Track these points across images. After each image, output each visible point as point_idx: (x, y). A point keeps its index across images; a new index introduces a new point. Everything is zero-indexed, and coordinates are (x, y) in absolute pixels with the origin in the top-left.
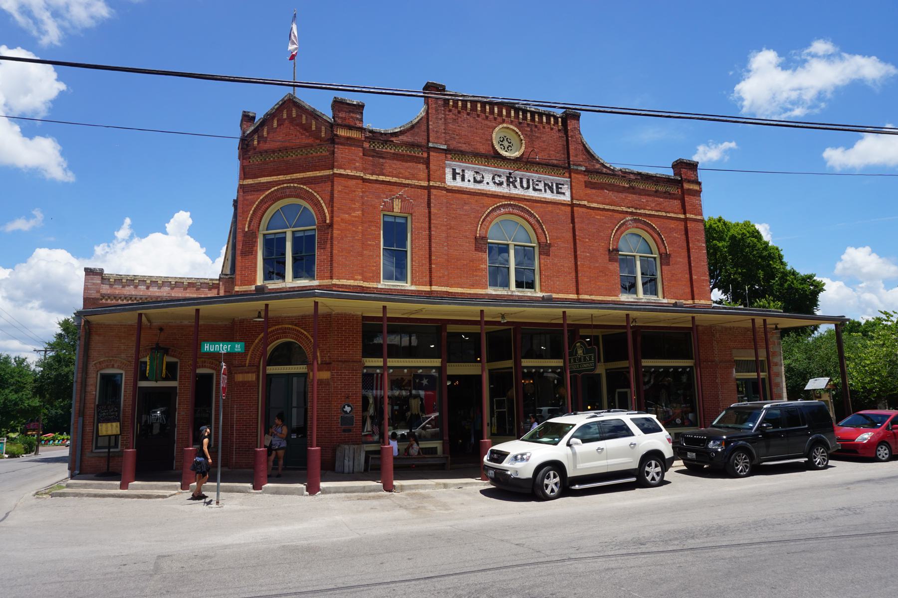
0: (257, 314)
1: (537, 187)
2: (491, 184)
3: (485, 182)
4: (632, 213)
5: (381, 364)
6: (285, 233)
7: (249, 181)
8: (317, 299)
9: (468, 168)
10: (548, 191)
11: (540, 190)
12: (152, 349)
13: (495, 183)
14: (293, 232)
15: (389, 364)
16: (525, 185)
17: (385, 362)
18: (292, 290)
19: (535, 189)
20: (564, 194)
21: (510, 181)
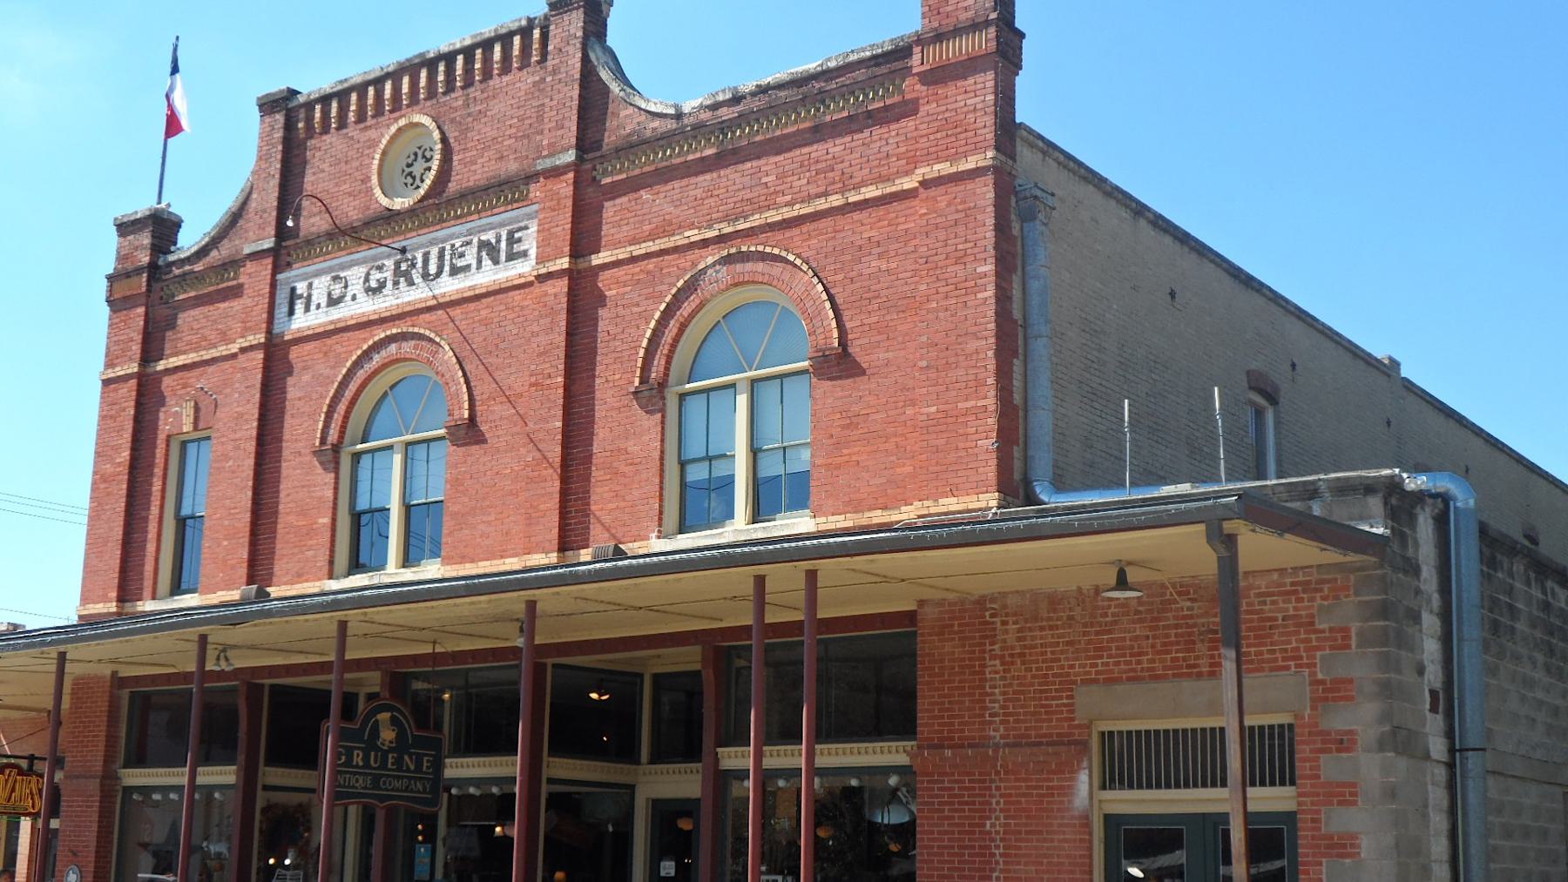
1: (460, 263)
2: (361, 297)
3: (348, 298)
10: (487, 262)
11: (468, 267)
16: (433, 269)
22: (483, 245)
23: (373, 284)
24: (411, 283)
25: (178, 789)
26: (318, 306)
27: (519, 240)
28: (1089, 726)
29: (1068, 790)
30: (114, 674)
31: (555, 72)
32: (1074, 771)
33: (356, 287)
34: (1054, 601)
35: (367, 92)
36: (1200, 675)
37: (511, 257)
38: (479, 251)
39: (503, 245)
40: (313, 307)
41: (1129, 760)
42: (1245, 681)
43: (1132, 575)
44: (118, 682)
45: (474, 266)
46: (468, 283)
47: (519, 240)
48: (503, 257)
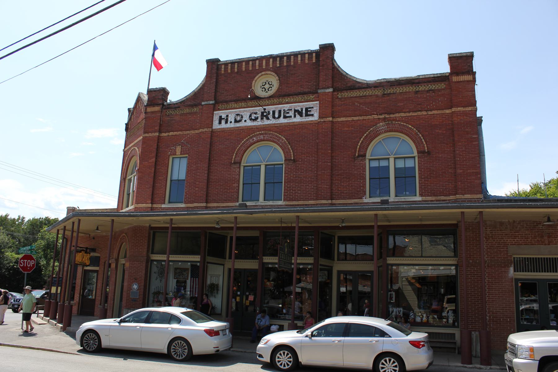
0: (546, 219)
1: (287, 115)
2: (248, 121)
3: (243, 121)
4: (384, 119)
5: (165, 259)
6: (260, 166)
7: (470, 109)
8: (80, 218)
9: (230, 113)
10: (298, 116)
11: (291, 117)
12: (406, 247)
13: (251, 119)
14: (266, 165)
15: (170, 259)
16: (277, 115)
17: (168, 257)
18: (263, 207)
19: (285, 117)
20: (312, 115)
21: (265, 115)
22: (295, 111)
23: (253, 118)
24: (268, 119)
25: (164, 261)
26: (231, 122)
27: (310, 111)
28: (511, 256)
29: (507, 272)
30: (150, 225)
31: (323, 66)
32: (509, 267)
33: (246, 117)
34: (501, 224)
35: (249, 64)
36: (545, 244)
37: (307, 115)
38: (295, 113)
39: (304, 111)
40: (229, 122)
41: (523, 265)
42: (71, 227)
43: (551, 218)
44: (151, 228)
45: (293, 116)
46: (291, 121)
47: (310, 111)
48: (304, 115)
